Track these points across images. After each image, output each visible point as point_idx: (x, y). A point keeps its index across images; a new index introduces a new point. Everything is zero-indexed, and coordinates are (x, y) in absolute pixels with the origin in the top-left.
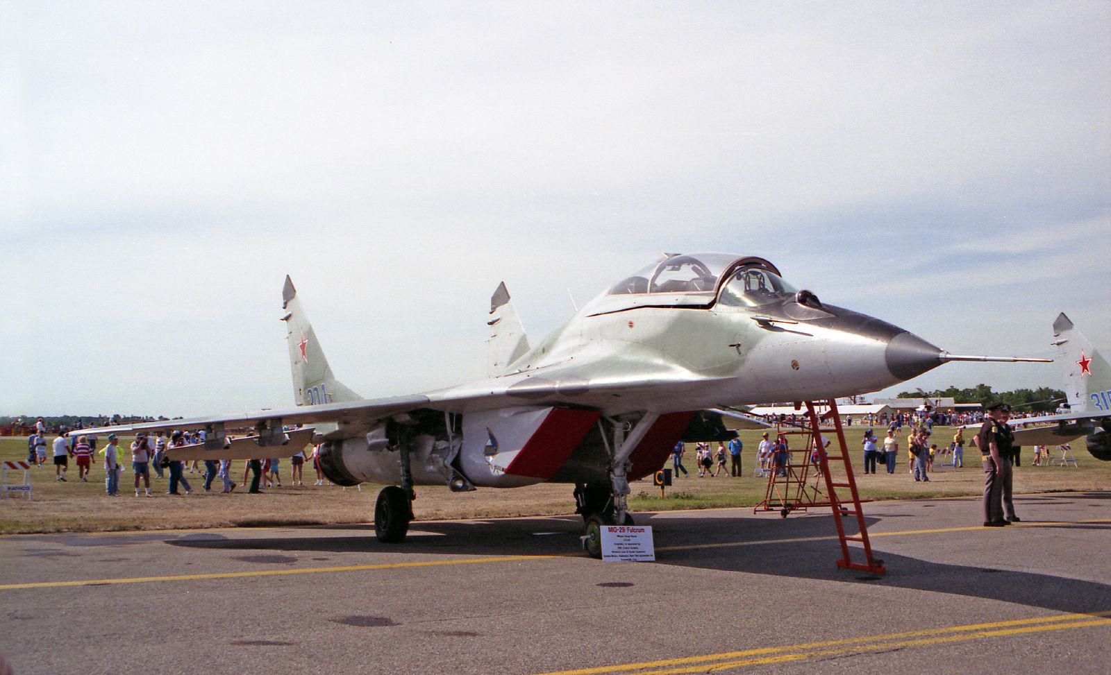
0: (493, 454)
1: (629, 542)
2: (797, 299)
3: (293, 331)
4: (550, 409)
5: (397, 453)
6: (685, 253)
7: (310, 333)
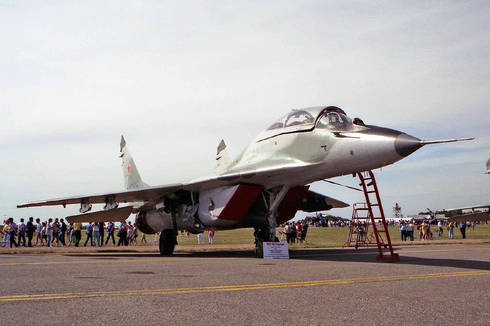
0: (212, 210)
1: (277, 250)
2: (353, 122)
3: (125, 162)
4: (238, 186)
5: (170, 214)
6: (299, 108)
7: (132, 162)
